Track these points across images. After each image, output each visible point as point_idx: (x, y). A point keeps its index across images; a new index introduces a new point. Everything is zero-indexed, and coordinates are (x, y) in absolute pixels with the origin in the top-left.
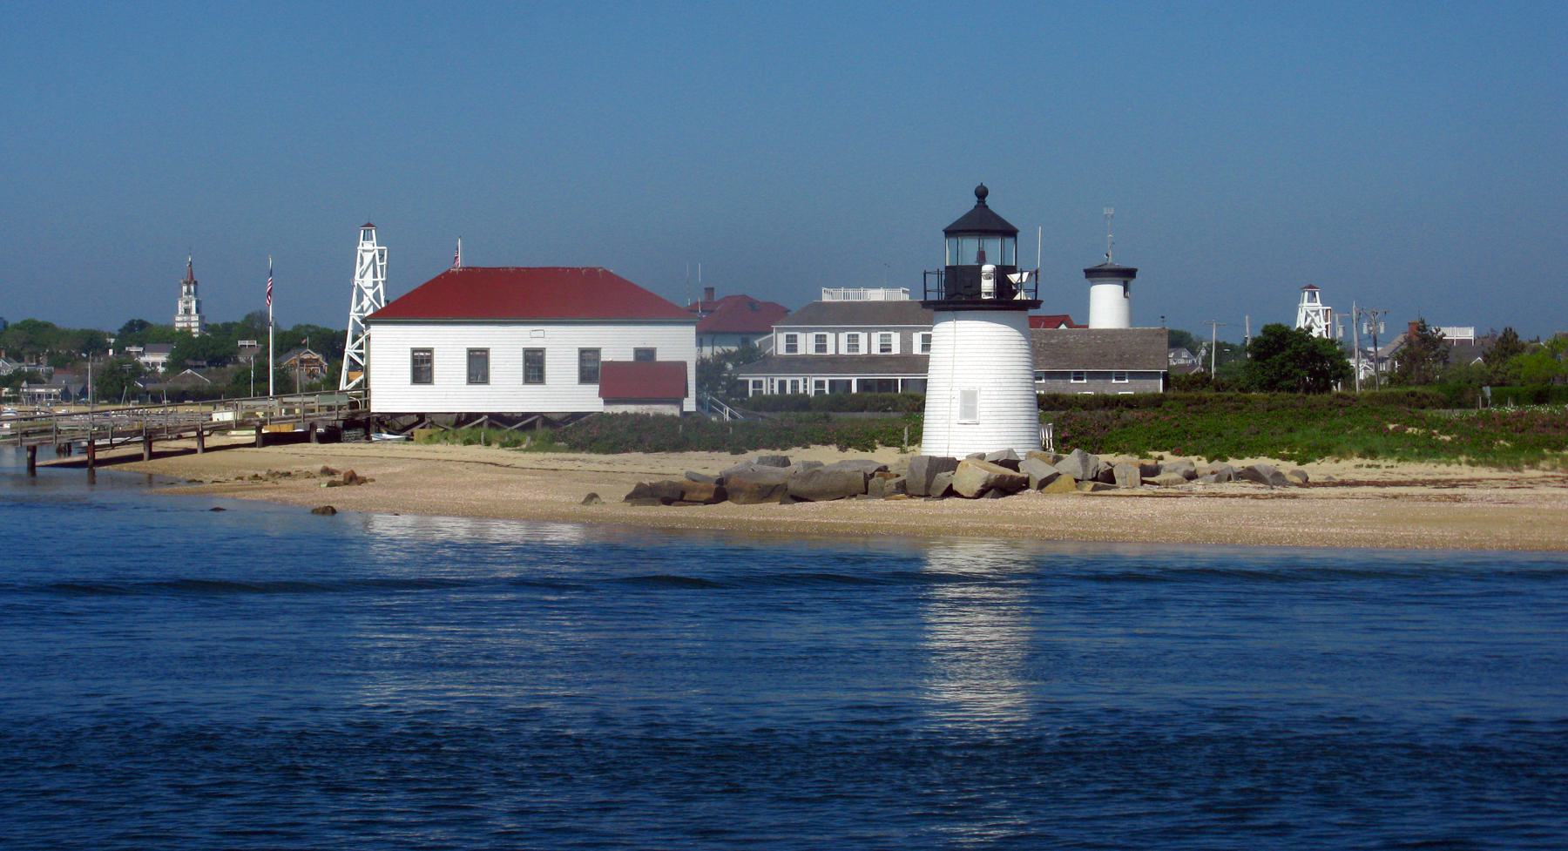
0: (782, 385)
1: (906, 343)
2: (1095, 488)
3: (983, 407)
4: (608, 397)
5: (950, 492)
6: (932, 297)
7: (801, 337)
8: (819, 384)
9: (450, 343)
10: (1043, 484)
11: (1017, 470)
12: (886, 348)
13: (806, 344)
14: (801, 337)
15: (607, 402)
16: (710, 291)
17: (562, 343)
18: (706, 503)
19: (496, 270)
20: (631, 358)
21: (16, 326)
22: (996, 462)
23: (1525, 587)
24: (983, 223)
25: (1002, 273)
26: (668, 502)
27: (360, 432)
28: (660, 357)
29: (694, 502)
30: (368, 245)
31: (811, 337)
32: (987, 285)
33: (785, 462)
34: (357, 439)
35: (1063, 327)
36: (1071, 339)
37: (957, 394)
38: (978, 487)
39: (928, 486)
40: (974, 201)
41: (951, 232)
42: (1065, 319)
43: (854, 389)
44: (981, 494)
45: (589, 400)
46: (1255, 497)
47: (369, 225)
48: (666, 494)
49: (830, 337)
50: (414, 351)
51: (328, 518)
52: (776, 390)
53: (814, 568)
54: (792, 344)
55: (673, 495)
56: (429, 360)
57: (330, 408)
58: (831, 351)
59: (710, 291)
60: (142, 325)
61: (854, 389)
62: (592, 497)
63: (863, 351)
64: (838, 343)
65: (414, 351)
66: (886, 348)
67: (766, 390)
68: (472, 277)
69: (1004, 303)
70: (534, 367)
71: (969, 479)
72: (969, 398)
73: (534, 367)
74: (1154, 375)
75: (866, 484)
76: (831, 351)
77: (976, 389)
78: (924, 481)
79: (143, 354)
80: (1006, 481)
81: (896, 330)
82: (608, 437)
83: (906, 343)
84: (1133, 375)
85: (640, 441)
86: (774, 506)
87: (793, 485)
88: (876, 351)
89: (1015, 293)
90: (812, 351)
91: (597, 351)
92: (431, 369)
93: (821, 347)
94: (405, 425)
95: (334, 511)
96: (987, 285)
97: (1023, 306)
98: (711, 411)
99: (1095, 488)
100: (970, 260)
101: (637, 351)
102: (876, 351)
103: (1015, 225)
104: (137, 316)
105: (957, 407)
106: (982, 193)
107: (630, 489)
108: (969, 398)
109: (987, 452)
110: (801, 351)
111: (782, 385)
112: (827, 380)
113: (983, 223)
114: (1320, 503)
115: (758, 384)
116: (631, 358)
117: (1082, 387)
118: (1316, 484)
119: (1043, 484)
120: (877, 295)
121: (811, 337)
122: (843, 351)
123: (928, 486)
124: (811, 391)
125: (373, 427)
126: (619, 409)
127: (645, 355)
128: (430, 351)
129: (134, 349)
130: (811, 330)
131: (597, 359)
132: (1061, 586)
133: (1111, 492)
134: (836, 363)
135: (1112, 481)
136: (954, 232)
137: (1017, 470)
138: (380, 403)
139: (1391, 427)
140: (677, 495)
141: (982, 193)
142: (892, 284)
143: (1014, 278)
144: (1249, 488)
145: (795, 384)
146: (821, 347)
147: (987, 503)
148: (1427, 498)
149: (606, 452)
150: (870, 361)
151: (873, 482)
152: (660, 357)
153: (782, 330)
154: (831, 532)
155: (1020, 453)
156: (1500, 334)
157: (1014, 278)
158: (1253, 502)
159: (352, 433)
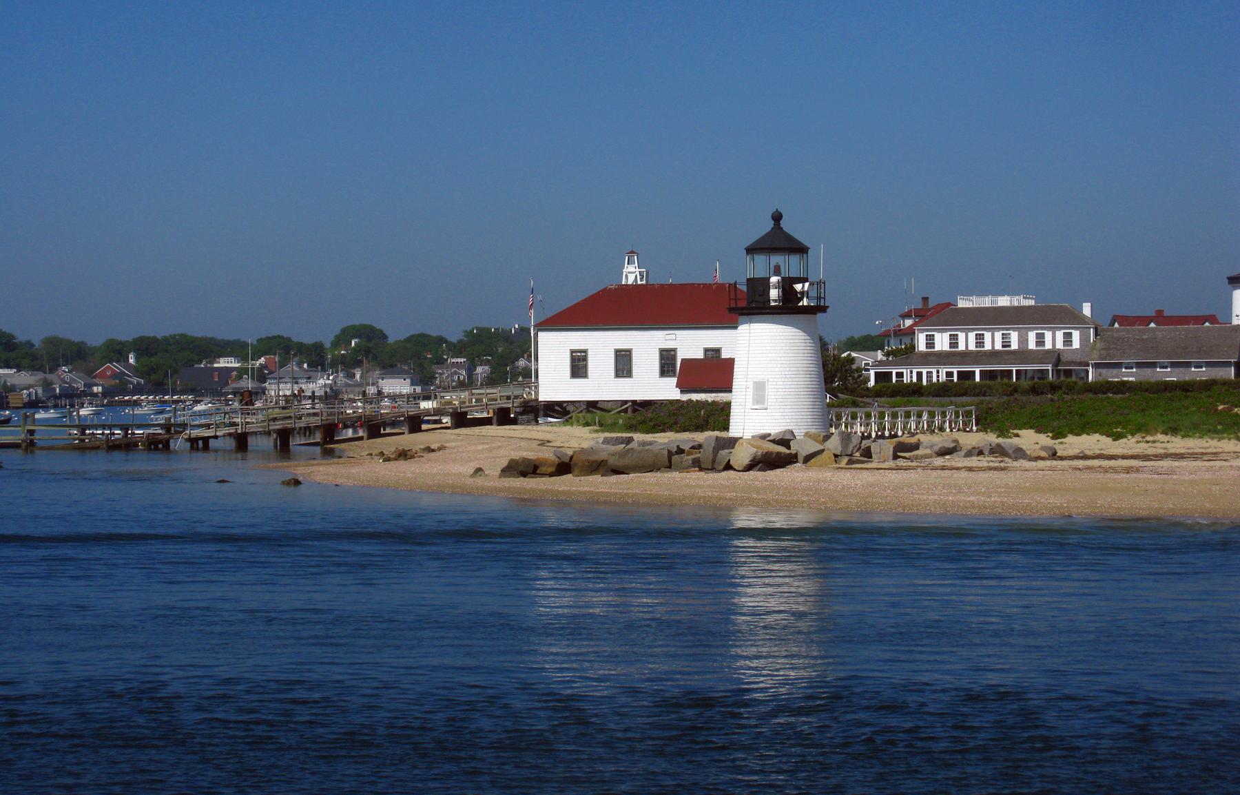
0: (919, 375)
1: (1023, 340)
2: (850, 462)
3: (771, 395)
4: (683, 387)
5: (728, 467)
7: (938, 336)
8: (949, 374)
9: (601, 344)
10: (808, 459)
11: (789, 448)
12: (1006, 344)
13: (942, 342)
14: (938, 336)
15: (682, 392)
16: (925, 299)
17: (646, 344)
18: (551, 475)
19: (692, 285)
20: (701, 355)
22: (773, 441)
23: (81, 553)
24: (778, 242)
25: (786, 286)
26: (524, 474)
27: (531, 416)
29: (543, 475)
30: (631, 268)
31: (946, 336)
32: (774, 293)
33: (630, 440)
34: (528, 422)
35: (1152, 325)
36: (1160, 334)
37: (751, 385)
38: (746, 461)
39: (714, 461)
40: (771, 224)
42: (1212, 319)
43: (978, 379)
44: (749, 468)
45: (667, 390)
46: (970, 469)
47: (632, 252)
48: (521, 468)
49: (962, 336)
50: (572, 352)
51: (292, 489)
52: (915, 380)
53: (381, 528)
54: (930, 342)
55: (528, 469)
56: (585, 359)
57: (508, 398)
58: (962, 347)
59: (925, 299)
61: (978, 379)
62: (479, 470)
63: (988, 347)
64: (966, 341)
65: (572, 352)
66: (1006, 344)
67: (906, 380)
69: (789, 308)
70: (623, 364)
71: (741, 456)
72: (760, 387)
73: (623, 364)
74: (1228, 364)
75: (670, 461)
76: (962, 347)
77: (769, 374)
78: (711, 457)
80: (776, 455)
81: (1014, 329)
82: (651, 420)
83: (1023, 340)
84: (1208, 364)
86: (597, 479)
88: (998, 346)
89: (801, 299)
90: (946, 347)
92: (586, 366)
93: (954, 344)
94: (558, 410)
95: (297, 483)
96: (774, 293)
99: (850, 462)
100: (760, 274)
101: (706, 350)
102: (998, 346)
103: (805, 241)
105: (750, 393)
106: (777, 217)
107: (504, 463)
108: (760, 387)
109: (773, 432)
110: (938, 348)
111: (919, 375)
112: (955, 371)
113: (778, 242)
114: (964, 474)
115: (900, 375)
116: (701, 355)
117: (1167, 374)
118: (1061, 458)
119: (808, 459)
120: (1004, 301)
121: (946, 336)
122: (972, 347)
123: (714, 461)
124: (943, 378)
125: (541, 413)
126: (695, 397)
128: (585, 351)
130: (946, 331)
132: (836, 544)
134: (966, 357)
137: (789, 448)
138: (547, 393)
139: (1221, 407)
140: (531, 470)
141: (777, 217)
142: (1025, 293)
143: (798, 287)
144: (993, 461)
145: (929, 374)
146: (954, 344)
148: (1128, 470)
149: (647, 432)
150: (993, 355)
151: (675, 458)
153: (923, 331)
154: (594, 501)
155: (799, 433)
157: (798, 287)
158: (970, 474)
159: (525, 417)
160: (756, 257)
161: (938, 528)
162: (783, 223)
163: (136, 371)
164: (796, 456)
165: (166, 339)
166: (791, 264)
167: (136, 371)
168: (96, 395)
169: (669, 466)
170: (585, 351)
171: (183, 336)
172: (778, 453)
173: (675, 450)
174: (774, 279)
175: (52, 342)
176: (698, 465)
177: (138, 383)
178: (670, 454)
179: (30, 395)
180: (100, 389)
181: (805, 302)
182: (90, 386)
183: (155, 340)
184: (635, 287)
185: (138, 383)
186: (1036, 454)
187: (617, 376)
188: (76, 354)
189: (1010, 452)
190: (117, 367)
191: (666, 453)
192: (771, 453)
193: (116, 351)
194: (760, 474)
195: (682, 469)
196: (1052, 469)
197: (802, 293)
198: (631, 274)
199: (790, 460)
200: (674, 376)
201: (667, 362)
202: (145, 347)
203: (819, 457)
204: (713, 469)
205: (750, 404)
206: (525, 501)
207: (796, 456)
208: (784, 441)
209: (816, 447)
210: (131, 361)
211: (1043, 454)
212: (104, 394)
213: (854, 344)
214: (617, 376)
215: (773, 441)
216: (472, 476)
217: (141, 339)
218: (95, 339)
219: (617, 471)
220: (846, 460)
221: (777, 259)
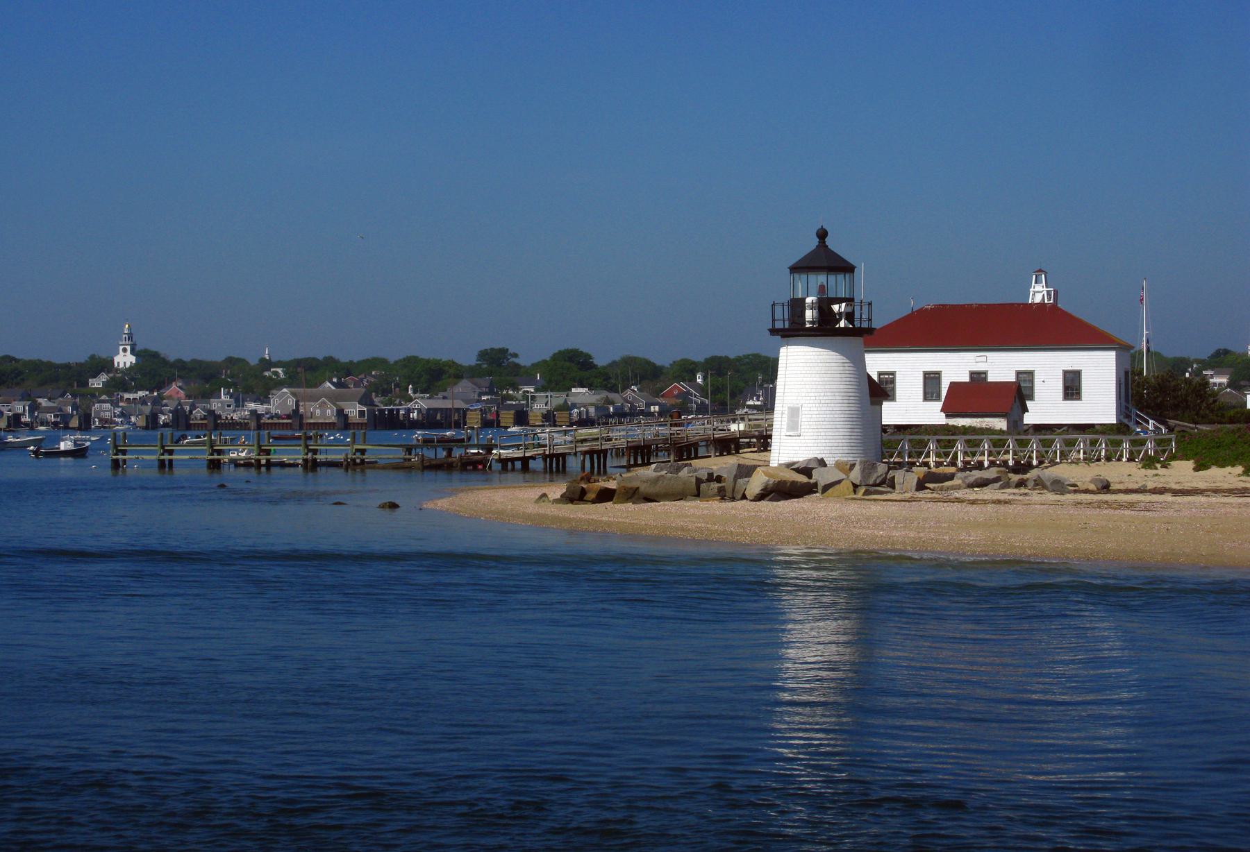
2: (867, 493)
3: (805, 420)
4: (948, 410)
5: (744, 497)
6: (779, 325)
10: (827, 488)
11: (810, 476)
15: (947, 416)
18: (593, 502)
20: (966, 379)
21: (396, 362)
24: (825, 260)
25: (824, 306)
28: (991, 378)
30: (1038, 288)
32: (809, 314)
40: (816, 241)
41: (795, 269)
44: (761, 497)
45: (933, 414)
56: (893, 381)
60: (1226, 352)
68: (942, 312)
79: (1212, 376)
80: (798, 485)
85: (919, 448)
87: (644, 488)
89: (838, 321)
91: (985, 373)
92: (893, 389)
97: (844, 332)
98: (1138, 423)
99: (867, 493)
101: (972, 374)
103: (851, 259)
104: (236, 355)
106: (822, 235)
108: (794, 412)
113: (825, 260)
114: (990, 507)
116: (966, 379)
119: (827, 488)
127: (978, 378)
128: (893, 374)
129: (1209, 372)
131: (986, 378)
133: (893, 496)
135: (893, 487)
136: (801, 268)
140: (577, 496)
141: (822, 235)
143: (836, 308)
147: (764, 504)
151: (703, 486)
152: (991, 378)
155: (830, 461)
156: (516, 360)
157: (836, 308)
160: (796, 276)
161: (1015, 564)
162: (828, 241)
163: (702, 390)
164: (816, 485)
165: (739, 359)
166: (837, 284)
167: (702, 390)
168: (652, 414)
169: (698, 494)
170: (893, 374)
171: (756, 356)
172: (793, 483)
173: (705, 477)
174: (809, 300)
175: (629, 361)
176: (723, 495)
177: (702, 403)
178: (699, 481)
179: (580, 414)
180: (657, 408)
181: (842, 324)
182: (648, 405)
183: (727, 359)
184: (1042, 305)
185: (702, 403)
186: (1084, 487)
187: (926, 399)
188: (645, 373)
189: (1048, 484)
190: (684, 386)
191: (694, 480)
192: (785, 482)
193: (686, 370)
194: (770, 503)
195: (708, 497)
196: (1100, 505)
197: (840, 314)
198: (1038, 293)
199: (809, 489)
200: (938, 399)
201: (931, 381)
202: (716, 366)
203: (837, 487)
204: (733, 499)
205: (784, 432)
206: (575, 531)
207: (816, 485)
208: (806, 471)
209: (842, 476)
210: (699, 381)
211: (1092, 487)
212: (661, 414)
213: (1205, 365)
214: (926, 399)
215: (798, 470)
216: (537, 501)
217: (713, 359)
218: (664, 358)
219: (648, 499)
220: (862, 490)
221: (822, 278)
